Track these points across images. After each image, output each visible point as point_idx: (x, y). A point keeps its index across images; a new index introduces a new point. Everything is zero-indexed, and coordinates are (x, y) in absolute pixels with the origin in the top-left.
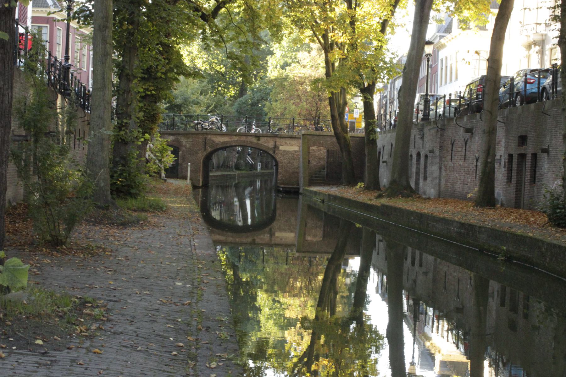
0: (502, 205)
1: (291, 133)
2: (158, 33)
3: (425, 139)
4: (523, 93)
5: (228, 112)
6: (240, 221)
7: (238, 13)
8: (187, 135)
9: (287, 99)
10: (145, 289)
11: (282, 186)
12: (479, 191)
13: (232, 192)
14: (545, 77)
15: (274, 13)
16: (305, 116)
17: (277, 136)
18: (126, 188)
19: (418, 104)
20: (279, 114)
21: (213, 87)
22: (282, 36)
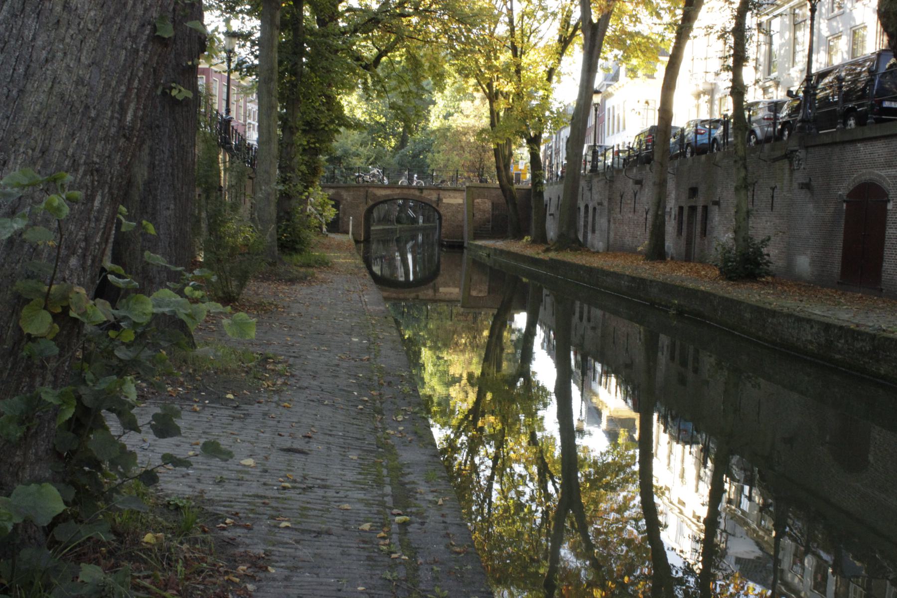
0: (672, 258)
1: (454, 186)
2: (322, 84)
3: (594, 191)
4: (694, 144)
5: (389, 164)
6: (402, 276)
7: (400, 62)
8: (347, 188)
9: (451, 150)
10: (322, 345)
11: (446, 240)
12: (650, 244)
13: (393, 246)
14: (716, 128)
15: (438, 62)
16: (468, 167)
17: (440, 189)
18: (291, 243)
19: (586, 155)
20: (442, 166)
21: (373, 139)
22: (445, 85)
